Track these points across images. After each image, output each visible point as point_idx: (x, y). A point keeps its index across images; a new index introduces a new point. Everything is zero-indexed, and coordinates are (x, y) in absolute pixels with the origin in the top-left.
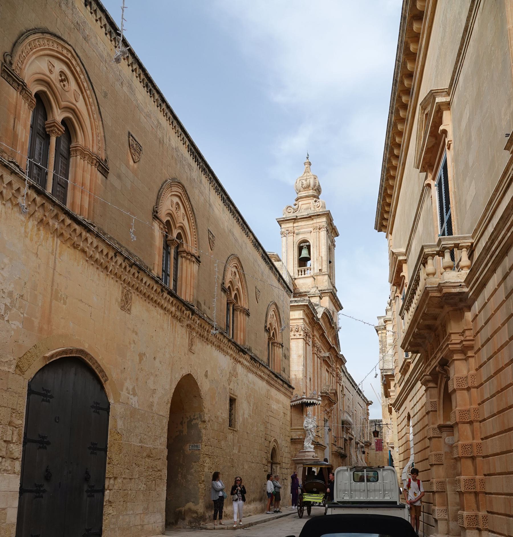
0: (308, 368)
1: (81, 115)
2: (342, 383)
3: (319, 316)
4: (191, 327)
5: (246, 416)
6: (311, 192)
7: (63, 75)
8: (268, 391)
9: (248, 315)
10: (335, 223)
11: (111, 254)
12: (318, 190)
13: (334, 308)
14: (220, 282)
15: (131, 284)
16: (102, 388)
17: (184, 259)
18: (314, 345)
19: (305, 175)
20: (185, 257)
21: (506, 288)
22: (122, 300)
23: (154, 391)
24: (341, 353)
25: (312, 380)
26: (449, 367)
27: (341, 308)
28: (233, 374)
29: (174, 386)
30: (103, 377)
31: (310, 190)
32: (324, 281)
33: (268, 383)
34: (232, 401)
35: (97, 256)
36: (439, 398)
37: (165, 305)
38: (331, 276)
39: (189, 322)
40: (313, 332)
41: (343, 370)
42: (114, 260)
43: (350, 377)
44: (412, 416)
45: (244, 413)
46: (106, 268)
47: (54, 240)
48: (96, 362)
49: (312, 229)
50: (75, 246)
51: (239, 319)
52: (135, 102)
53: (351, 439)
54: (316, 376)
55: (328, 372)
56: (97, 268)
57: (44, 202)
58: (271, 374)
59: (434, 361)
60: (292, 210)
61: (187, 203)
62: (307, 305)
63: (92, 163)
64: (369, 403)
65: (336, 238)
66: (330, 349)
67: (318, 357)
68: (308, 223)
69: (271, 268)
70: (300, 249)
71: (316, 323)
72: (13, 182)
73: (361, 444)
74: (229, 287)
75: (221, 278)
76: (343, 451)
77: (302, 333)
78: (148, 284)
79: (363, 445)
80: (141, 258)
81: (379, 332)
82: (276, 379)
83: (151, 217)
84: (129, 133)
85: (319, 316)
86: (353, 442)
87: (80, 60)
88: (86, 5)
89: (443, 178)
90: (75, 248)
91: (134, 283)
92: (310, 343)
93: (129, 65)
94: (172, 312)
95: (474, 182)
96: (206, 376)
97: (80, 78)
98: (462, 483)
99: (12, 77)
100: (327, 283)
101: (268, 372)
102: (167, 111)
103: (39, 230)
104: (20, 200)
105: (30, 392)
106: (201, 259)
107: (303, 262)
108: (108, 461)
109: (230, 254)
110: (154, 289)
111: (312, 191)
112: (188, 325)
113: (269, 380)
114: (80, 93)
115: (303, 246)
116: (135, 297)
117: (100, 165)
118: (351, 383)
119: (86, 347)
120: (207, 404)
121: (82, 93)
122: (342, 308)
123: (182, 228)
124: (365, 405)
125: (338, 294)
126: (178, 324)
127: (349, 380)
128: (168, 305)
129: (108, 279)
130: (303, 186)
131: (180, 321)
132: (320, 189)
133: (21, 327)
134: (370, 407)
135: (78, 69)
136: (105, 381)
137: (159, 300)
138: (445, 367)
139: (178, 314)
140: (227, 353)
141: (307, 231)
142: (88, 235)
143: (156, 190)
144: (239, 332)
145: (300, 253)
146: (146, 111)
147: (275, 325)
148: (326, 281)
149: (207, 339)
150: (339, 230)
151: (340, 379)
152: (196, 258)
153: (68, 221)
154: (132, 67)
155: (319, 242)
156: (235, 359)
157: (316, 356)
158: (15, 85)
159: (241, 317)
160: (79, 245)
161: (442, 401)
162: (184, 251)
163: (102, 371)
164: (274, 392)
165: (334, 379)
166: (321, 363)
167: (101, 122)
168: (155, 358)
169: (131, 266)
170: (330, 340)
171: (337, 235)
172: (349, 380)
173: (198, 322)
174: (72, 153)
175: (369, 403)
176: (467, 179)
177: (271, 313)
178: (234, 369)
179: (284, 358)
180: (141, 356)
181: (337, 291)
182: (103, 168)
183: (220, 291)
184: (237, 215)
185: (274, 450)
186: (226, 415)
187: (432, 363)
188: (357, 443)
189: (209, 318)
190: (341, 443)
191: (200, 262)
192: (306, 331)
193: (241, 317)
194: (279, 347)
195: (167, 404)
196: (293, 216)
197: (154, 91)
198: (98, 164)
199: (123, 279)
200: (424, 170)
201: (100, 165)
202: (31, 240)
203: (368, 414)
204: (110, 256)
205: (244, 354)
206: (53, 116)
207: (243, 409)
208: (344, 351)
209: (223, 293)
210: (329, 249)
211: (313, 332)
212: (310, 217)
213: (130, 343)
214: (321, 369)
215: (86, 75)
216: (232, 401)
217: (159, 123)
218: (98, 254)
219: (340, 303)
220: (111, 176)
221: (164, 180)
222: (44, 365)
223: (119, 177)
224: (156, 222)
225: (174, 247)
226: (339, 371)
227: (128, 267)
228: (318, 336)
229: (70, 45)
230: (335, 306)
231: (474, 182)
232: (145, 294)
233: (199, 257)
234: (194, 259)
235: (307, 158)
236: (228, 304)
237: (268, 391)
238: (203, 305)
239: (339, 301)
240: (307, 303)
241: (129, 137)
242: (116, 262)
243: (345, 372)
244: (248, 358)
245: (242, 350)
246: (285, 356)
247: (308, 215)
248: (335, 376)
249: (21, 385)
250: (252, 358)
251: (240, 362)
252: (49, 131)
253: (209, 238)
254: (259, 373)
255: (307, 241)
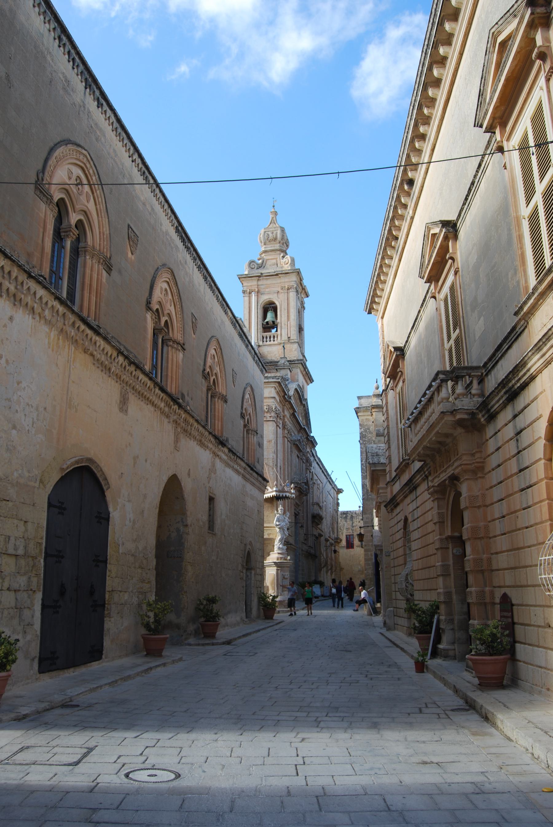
0: (279, 455)
1: (92, 217)
2: (313, 470)
3: (291, 393)
4: (176, 422)
5: (223, 517)
6: (277, 246)
7: (78, 179)
8: (244, 486)
9: (226, 401)
10: (305, 282)
11: (115, 354)
12: (286, 243)
13: (304, 381)
14: (202, 369)
15: (129, 384)
16: (104, 496)
17: (174, 350)
18: (284, 427)
19: (271, 226)
20: (171, 346)
21: (515, 427)
22: (120, 402)
23: (145, 496)
24: (312, 435)
25: (282, 469)
26: (460, 483)
27: (312, 381)
28: (213, 470)
29: (162, 489)
30: (106, 485)
31: (277, 243)
32: (294, 350)
33: (244, 477)
34: (211, 499)
35: (103, 358)
36: (447, 510)
37: (156, 402)
38: (301, 344)
39: (175, 417)
40: (283, 412)
41: (313, 454)
42: (116, 361)
43: (320, 461)
44: (410, 519)
45: (221, 514)
46: (110, 369)
47: (69, 347)
48: (101, 470)
49: (279, 290)
50: (85, 351)
51: (217, 406)
52: (133, 193)
53: (321, 535)
54: (286, 463)
55: (298, 457)
56: (102, 371)
57: (65, 311)
58: (247, 467)
59: (444, 474)
60: (256, 266)
61: (174, 288)
62: (279, 383)
63: (99, 262)
64: (340, 491)
65: (306, 300)
66: (300, 430)
67: (288, 441)
68: (274, 282)
69: (247, 346)
70: (265, 310)
71: (287, 401)
72: (43, 296)
73: (331, 541)
74: (208, 372)
75: (202, 363)
76: (312, 551)
77: (273, 414)
78: (142, 382)
79: (333, 542)
80: (137, 355)
81: (359, 414)
82: (251, 472)
83: (144, 309)
84: (129, 225)
85: (291, 393)
86: (322, 539)
87: (93, 162)
88: (98, 107)
89: (449, 297)
90: (85, 352)
91: (131, 381)
92: (281, 426)
93: (130, 157)
94: (161, 409)
95: (482, 318)
96: (189, 475)
97: (92, 179)
98: (474, 595)
99: (43, 193)
100: (296, 352)
101: (244, 465)
102: (159, 195)
103: (59, 339)
104: (47, 313)
105: (50, 505)
106: (185, 347)
107: (268, 327)
108: (108, 573)
109: (210, 336)
110: (148, 386)
111: (278, 245)
112: (173, 421)
113: (245, 474)
114: (91, 194)
115: (269, 307)
116: (133, 399)
117: (106, 263)
118: (321, 468)
119: (91, 455)
120: (190, 506)
121: (93, 193)
122: (313, 381)
123: (169, 315)
124: (335, 493)
125: (308, 364)
126: (166, 420)
127: (319, 465)
128: (158, 401)
129: (110, 379)
130: (269, 239)
131: (168, 417)
132: (288, 242)
133: (44, 440)
134: (340, 496)
135: (91, 171)
136: (107, 489)
137: (151, 397)
138: (455, 482)
139: (167, 409)
140: (207, 447)
141: (272, 292)
142: (97, 338)
143: (149, 279)
144: (217, 422)
145: (265, 317)
146: (142, 198)
147: (250, 410)
148: (295, 350)
149: (190, 434)
150: (309, 289)
151: (311, 465)
152: (182, 346)
153: (83, 327)
154: (132, 157)
155: (286, 304)
156: (214, 453)
157: (286, 439)
158: (45, 199)
159: (219, 404)
160: (89, 350)
161: (450, 513)
162: (170, 340)
163: (106, 479)
164: (249, 487)
165: (304, 465)
166: (291, 448)
167: (107, 220)
168: (146, 461)
169: (129, 365)
170: (300, 419)
171: (307, 296)
172: (319, 465)
173: (183, 416)
174: (80, 253)
175: (340, 491)
176: (476, 311)
177: (247, 396)
178: (213, 465)
179: (258, 446)
180: (136, 458)
181: (306, 361)
182: (108, 266)
183: (201, 377)
184: (217, 293)
185: (249, 553)
186: (205, 518)
187: (441, 476)
188: (327, 540)
189: (192, 411)
190: (311, 542)
191: (185, 350)
192: (278, 412)
193: (219, 404)
194: (254, 435)
195: (156, 509)
196: (258, 273)
197: (150, 178)
198: (104, 263)
199: (122, 379)
200: (429, 281)
201: (106, 263)
202: (53, 350)
203: (338, 504)
204: (113, 357)
205: (222, 446)
206: (68, 221)
207: (222, 507)
208: (315, 433)
209: (203, 380)
210: (299, 312)
211: (283, 412)
212: (277, 275)
213: (126, 446)
214: (291, 454)
215: (92, 163)
216: (211, 499)
217: (153, 209)
218: (103, 356)
219: (310, 375)
220: (114, 273)
221: (156, 267)
222: (60, 477)
223: (120, 272)
224: (149, 313)
225: (162, 336)
226: (309, 455)
227: (127, 366)
228: (288, 415)
229: (86, 150)
230: (305, 379)
231: (482, 318)
232: (139, 392)
233: (184, 344)
234: (180, 348)
235: (274, 207)
236: (207, 391)
237: (244, 486)
238: (186, 397)
239: (309, 373)
240: (279, 380)
241: (129, 230)
242: (118, 363)
243: (314, 456)
244: (226, 450)
245: (222, 443)
246: (259, 445)
247: (275, 272)
248: (304, 461)
249: (42, 499)
250: (230, 450)
251: (218, 456)
252: (64, 236)
253: (193, 322)
254: (236, 466)
255: (274, 303)
